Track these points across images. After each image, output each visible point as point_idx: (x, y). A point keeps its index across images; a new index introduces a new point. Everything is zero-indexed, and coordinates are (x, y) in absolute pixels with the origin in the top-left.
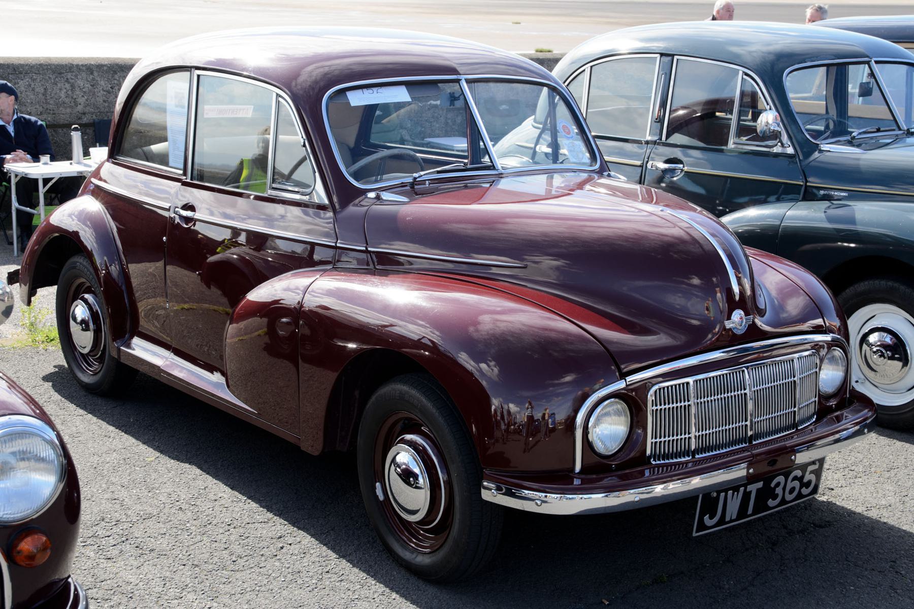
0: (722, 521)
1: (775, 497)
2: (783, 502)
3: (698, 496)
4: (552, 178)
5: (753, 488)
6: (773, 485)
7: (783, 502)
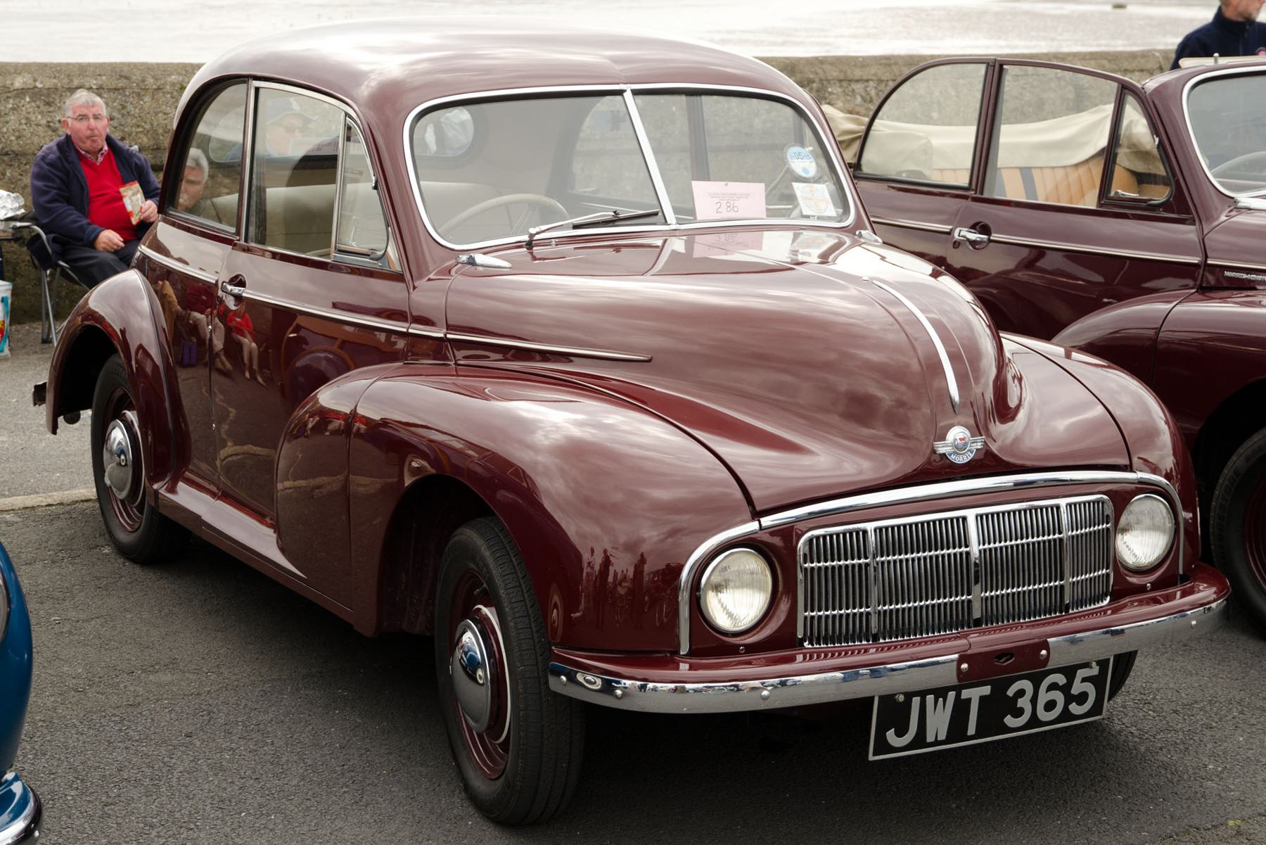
0: (920, 740)
1: (1018, 713)
2: (1034, 721)
3: (1109, 660)
4: (1166, 184)
5: (974, 694)
6: (1011, 692)
7: (1034, 721)
